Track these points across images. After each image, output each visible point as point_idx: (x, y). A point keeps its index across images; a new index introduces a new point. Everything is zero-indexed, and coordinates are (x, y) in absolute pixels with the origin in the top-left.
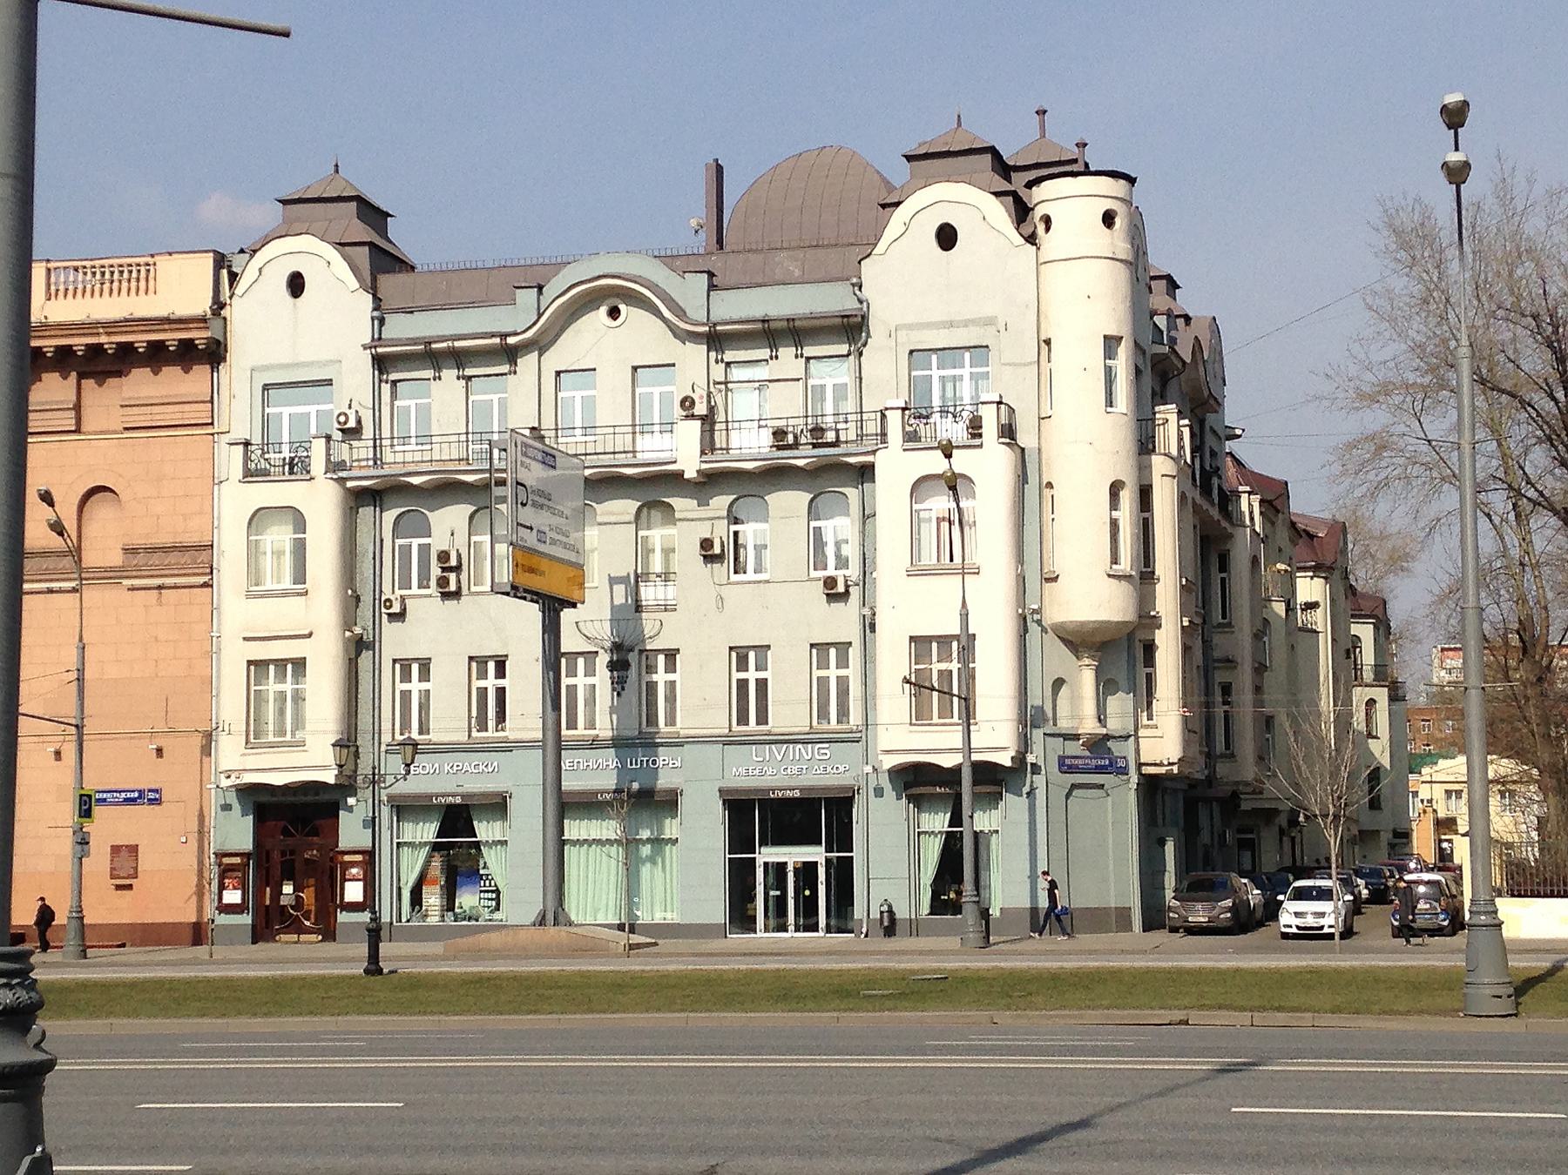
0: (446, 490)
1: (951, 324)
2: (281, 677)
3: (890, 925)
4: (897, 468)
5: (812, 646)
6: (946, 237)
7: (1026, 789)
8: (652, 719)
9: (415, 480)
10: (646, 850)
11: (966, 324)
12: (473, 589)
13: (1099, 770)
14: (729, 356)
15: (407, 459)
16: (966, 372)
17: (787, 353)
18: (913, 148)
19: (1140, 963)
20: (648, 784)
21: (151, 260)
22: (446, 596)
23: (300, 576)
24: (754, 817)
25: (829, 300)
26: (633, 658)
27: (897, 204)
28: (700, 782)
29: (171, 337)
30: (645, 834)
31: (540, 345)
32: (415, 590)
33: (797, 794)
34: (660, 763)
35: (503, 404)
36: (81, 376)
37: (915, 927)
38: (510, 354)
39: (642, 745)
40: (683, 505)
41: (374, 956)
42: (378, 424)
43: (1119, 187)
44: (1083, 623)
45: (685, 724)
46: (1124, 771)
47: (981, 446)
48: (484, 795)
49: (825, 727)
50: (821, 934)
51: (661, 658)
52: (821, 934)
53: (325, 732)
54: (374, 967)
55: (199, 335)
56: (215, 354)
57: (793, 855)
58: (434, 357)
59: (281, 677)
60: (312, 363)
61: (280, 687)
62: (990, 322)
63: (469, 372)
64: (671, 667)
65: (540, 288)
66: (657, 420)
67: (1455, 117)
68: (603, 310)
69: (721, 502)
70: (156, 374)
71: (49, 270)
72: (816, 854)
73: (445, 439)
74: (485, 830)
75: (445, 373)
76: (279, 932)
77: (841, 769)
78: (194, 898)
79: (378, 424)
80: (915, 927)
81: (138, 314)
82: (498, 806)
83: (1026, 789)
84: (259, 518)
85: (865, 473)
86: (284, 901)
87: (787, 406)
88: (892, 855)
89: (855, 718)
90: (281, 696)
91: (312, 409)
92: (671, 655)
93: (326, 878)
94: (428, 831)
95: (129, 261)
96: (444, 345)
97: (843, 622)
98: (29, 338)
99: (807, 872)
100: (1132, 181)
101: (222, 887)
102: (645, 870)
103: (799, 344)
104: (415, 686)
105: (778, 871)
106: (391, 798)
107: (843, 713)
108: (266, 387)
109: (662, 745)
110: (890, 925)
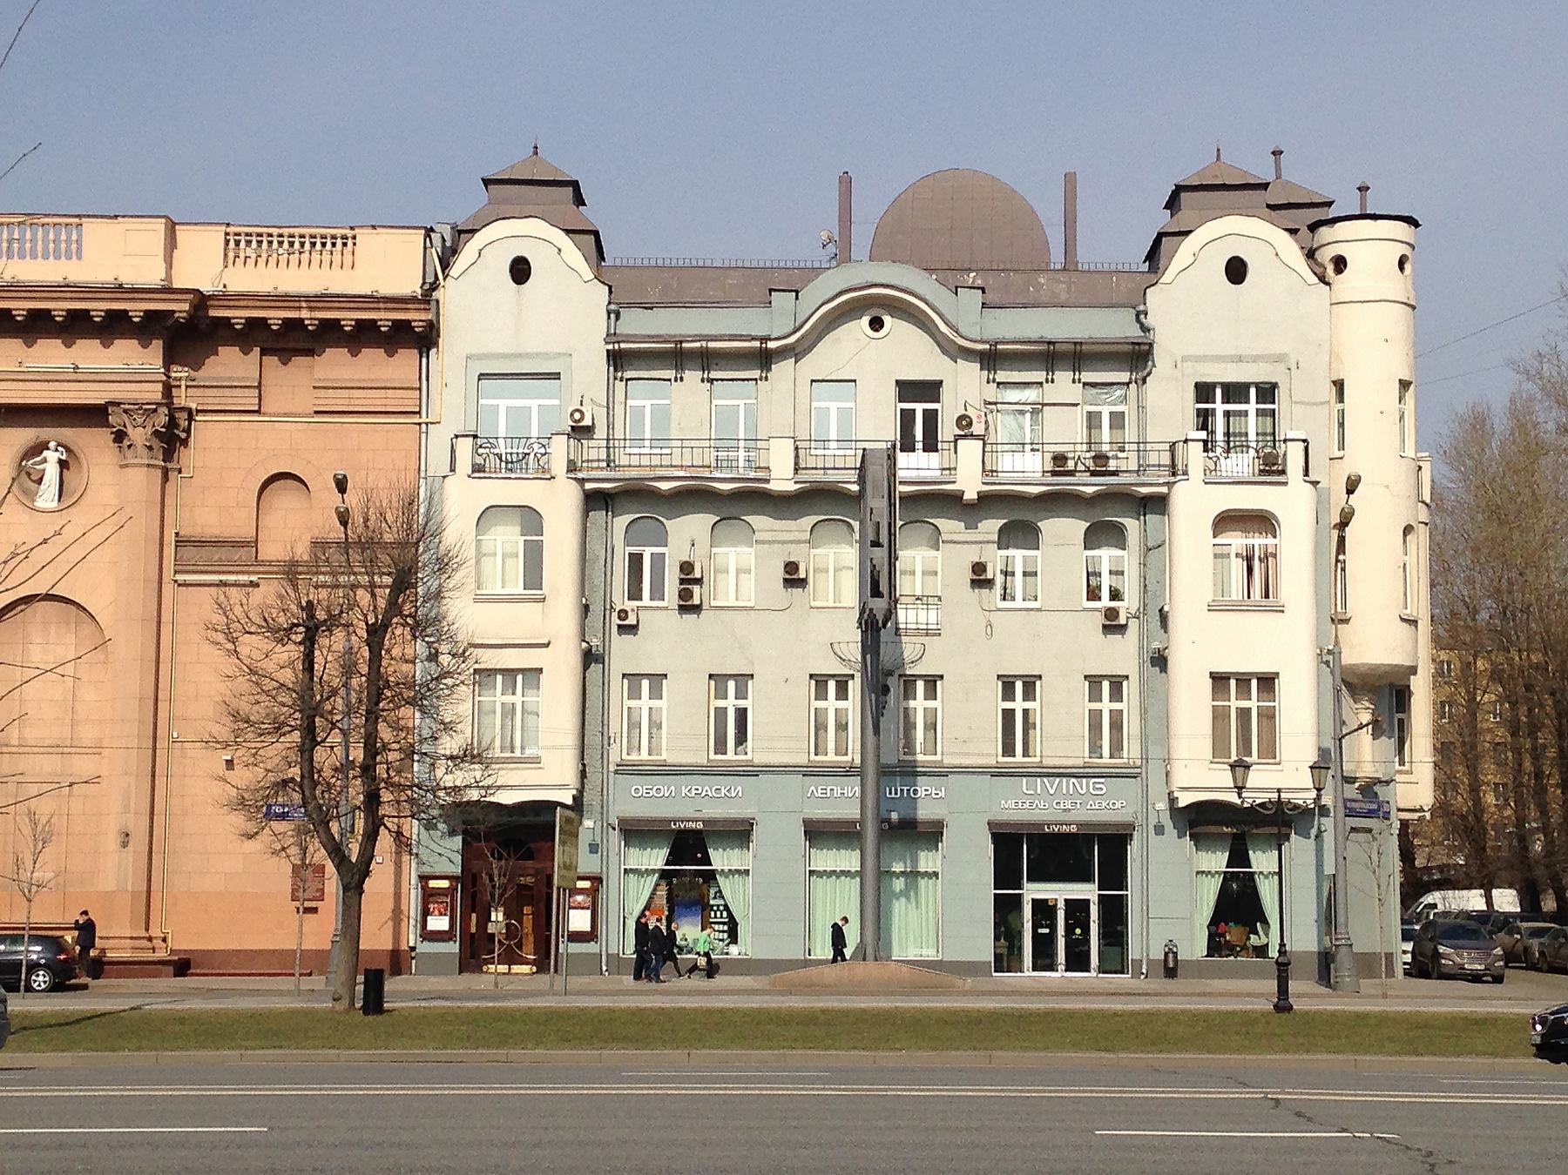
0: (694, 497)
1: (1240, 359)
2: (1244, 692)
3: (1171, 968)
4: (1195, 505)
5: (811, 676)
6: (1236, 270)
7: (1314, 832)
8: (909, 746)
9: (665, 486)
10: (899, 884)
11: (1256, 359)
12: (713, 603)
13: (1370, 814)
14: (1002, 376)
15: (635, 461)
16: (1252, 407)
17: (1063, 377)
18: (488, 175)
19: (755, 1003)
20: (907, 814)
21: (350, 233)
22: (684, 609)
23: (533, 577)
24: (1022, 852)
25: (1114, 326)
26: (892, 682)
27: (1188, 233)
28: (966, 818)
29: (384, 317)
30: (898, 867)
31: (796, 352)
32: (646, 600)
33: (1074, 829)
34: (921, 793)
35: (751, 413)
36: (264, 352)
37: (1199, 970)
38: (764, 359)
39: (902, 774)
40: (949, 526)
41: (1283, 990)
42: (610, 426)
43: (1400, 230)
44: (1378, 666)
45: (948, 752)
46: (1387, 816)
47: (1285, 484)
48: (726, 821)
49: (634, 757)
50: (1093, 974)
51: (920, 685)
52: (1028, 971)
53: (561, 748)
54: (1283, 1006)
55: (417, 317)
56: (425, 339)
57: (1059, 893)
58: (679, 357)
59: (1244, 692)
60: (538, 354)
61: (509, 699)
62: (1279, 359)
63: (713, 375)
64: (931, 693)
65: (797, 292)
66: (833, 436)
67: (1363, 189)
68: (866, 320)
69: (991, 526)
70: (354, 355)
71: (227, 234)
72: (1088, 892)
73: (697, 444)
74: (720, 859)
75: (687, 374)
76: (487, 962)
77: (1118, 805)
78: (391, 923)
79: (610, 426)
80: (1199, 970)
81: (335, 289)
82: (739, 833)
83: (1314, 832)
84: (489, 515)
85: (1157, 504)
86: (491, 929)
87: (1066, 430)
88: (1173, 893)
89: (1132, 751)
90: (1244, 714)
91: (534, 404)
92: (932, 682)
93: (542, 906)
94: (656, 858)
95: (303, 231)
96: (698, 345)
97: (1122, 655)
98: (207, 308)
99: (1077, 909)
100: (1416, 224)
101: (426, 913)
102: (899, 907)
103: (705, 368)
104: (645, 703)
105: (1044, 910)
106: (622, 821)
107: (1116, 748)
108: (482, 376)
109: (924, 774)
110: (1171, 968)
